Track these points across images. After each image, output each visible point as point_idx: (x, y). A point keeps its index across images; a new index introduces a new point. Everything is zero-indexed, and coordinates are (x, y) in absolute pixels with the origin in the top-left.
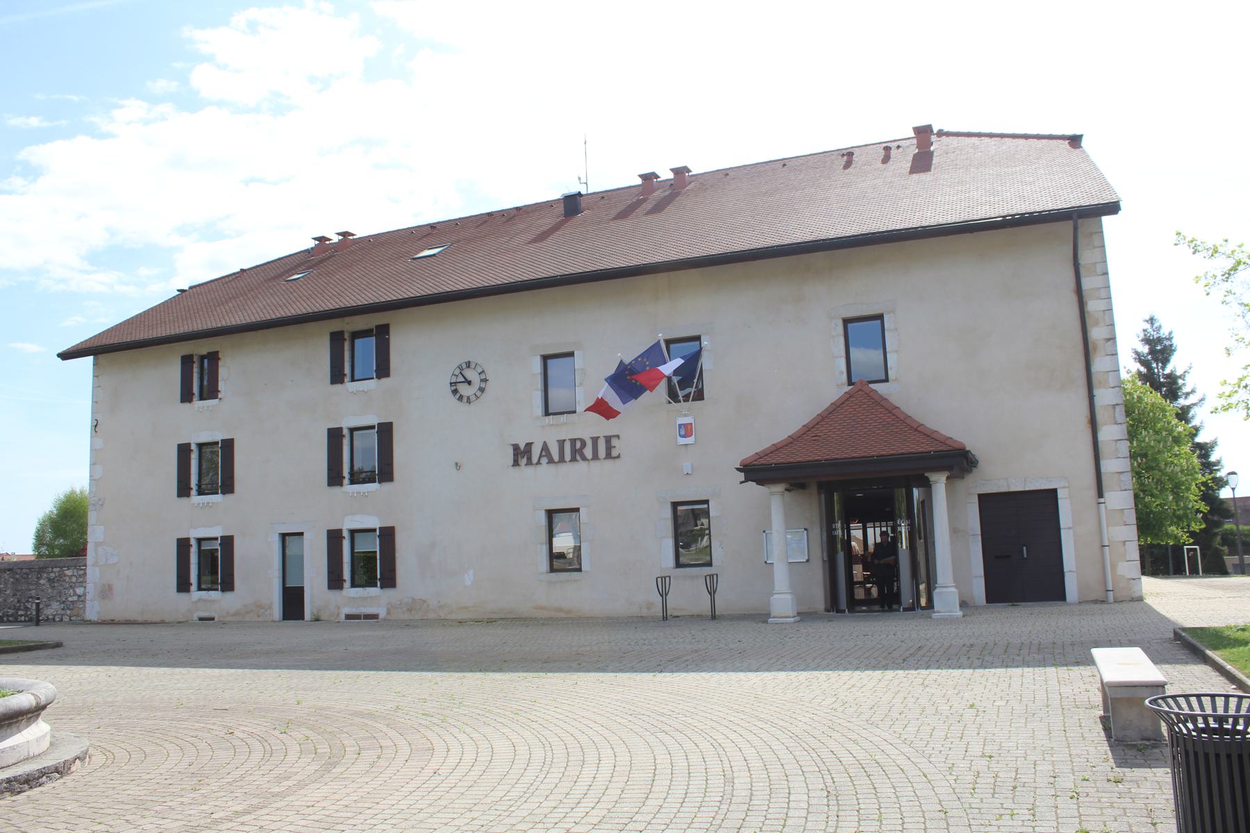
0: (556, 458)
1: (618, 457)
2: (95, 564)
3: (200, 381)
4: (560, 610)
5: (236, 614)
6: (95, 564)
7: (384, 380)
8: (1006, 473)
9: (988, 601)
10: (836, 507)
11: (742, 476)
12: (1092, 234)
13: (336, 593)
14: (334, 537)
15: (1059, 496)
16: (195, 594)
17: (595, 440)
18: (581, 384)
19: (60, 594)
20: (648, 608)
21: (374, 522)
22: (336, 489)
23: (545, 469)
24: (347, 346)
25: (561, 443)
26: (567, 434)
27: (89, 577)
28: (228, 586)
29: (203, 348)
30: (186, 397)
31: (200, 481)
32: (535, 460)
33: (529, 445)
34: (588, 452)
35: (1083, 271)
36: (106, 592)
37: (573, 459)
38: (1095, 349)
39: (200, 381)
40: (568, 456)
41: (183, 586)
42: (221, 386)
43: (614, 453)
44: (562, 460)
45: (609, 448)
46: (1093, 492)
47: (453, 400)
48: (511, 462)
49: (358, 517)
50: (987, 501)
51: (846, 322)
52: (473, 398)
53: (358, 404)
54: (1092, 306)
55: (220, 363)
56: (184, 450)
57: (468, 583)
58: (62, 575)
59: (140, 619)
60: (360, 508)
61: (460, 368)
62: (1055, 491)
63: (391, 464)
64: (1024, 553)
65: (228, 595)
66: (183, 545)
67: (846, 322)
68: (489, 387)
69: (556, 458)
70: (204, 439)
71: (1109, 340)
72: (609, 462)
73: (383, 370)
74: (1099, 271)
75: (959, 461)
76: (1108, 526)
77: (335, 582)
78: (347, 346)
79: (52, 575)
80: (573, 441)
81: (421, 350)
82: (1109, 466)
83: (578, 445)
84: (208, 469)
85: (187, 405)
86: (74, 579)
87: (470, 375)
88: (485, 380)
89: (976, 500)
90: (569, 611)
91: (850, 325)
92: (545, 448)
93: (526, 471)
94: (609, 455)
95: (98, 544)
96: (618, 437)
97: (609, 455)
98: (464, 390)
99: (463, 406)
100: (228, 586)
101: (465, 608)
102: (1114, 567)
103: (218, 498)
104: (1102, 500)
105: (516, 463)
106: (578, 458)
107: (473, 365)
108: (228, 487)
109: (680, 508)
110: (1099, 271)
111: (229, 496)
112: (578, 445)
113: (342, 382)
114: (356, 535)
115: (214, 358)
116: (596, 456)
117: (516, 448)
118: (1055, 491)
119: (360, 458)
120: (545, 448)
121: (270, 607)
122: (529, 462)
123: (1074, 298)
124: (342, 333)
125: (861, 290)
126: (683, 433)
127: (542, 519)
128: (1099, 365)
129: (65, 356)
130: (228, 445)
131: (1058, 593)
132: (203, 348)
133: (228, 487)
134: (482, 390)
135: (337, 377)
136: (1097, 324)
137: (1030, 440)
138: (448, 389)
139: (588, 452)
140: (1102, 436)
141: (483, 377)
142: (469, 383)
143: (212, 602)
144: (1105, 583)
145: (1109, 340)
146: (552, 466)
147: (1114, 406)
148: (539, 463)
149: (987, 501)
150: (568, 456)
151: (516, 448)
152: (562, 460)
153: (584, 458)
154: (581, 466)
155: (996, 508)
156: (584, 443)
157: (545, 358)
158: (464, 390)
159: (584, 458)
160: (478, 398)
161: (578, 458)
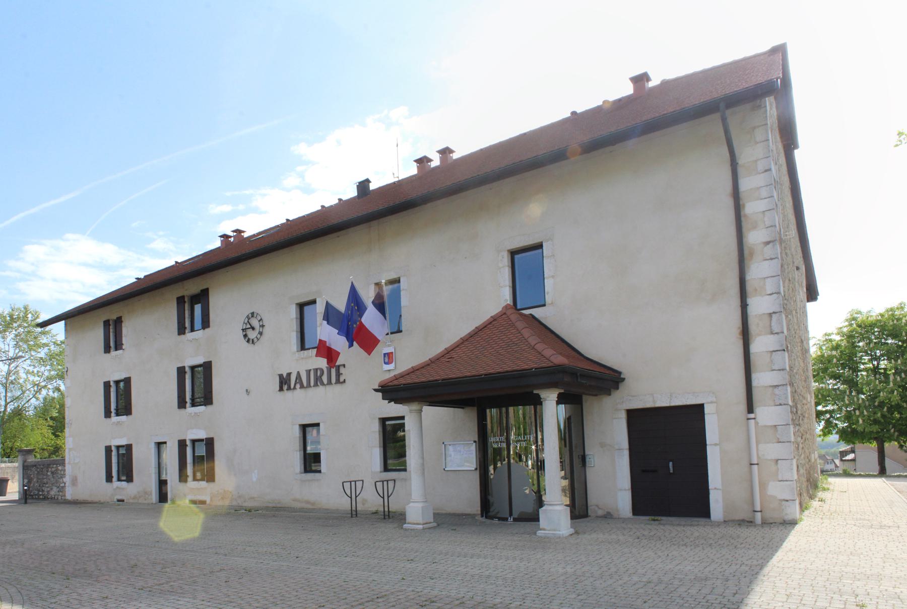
0: (305, 384)
1: (344, 381)
3: (113, 341)
4: (308, 502)
5: (134, 498)
6: (69, 463)
7: (207, 330)
8: (655, 386)
9: (638, 509)
12: (754, 128)
14: (182, 444)
15: (706, 410)
19: (57, 482)
20: (363, 504)
21: (202, 435)
22: (183, 411)
23: (299, 392)
24: (187, 306)
25: (308, 372)
27: (67, 472)
28: (130, 479)
29: (192, 288)
30: (107, 349)
32: (292, 386)
33: (289, 374)
34: (325, 379)
35: (741, 171)
36: (74, 481)
37: (316, 385)
38: (751, 254)
39: (113, 341)
41: (109, 478)
42: (124, 341)
43: (342, 380)
46: (743, 407)
48: (278, 388)
49: (194, 431)
50: (634, 416)
51: (513, 253)
52: (255, 340)
53: (192, 350)
55: (123, 325)
56: (107, 385)
57: (254, 479)
58: (57, 470)
59: (89, 499)
60: (194, 424)
61: (248, 317)
62: (701, 406)
63: (211, 392)
65: (131, 484)
66: (108, 450)
67: (513, 253)
68: (266, 330)
70: (117, 378)
72: (338, 387)
73: (206, 324)
75: (607, 380)
76: (758, 443)
77: (183, 477)
78: (187, 306)
81: (228, 303)
84: (120, 399)
85: (107, 355)
87: (255, 322)
88: (263, 326)
89: (623, 416)
90: (313, 504)
91: (516, 257)
92: (298, 373)
93: (288, 394)
95: (70, 450)
96: (344, 366)
97: (338, 381)
98: (252, 335)
99: (250, 346)
100: (130, 479)
101: (253, 498)
102: (763, 486)
104: (752, 416)
105: (281, 389)
109: (387, 423)
113: (184, 333)
115: (119, 321)
116: (330, 383)
117: (281, 376)
118: (701, 406)
119: (197, 385)
120: (298, 373)
121: (151, 494)
122: (289, 388)
123: (730, 202)
124: (183, 297)
125: (532, 215)
126: (387, 360)
127: (297, 432)
132: (192, 288)
133: (207, 400)
134: (261, 333)
135: (181, 330)
136: (755, 227)
138: (241, 334)
139: (325, 379)
140: (755, 348)
142: (253, 328)
143: (123, 489)
144: (752, 503)
147: (770, 315)
148: (295, 388)
149: (634, 416)
150: (312, 383)
151: (281, 376)
153: (323, 384)
154: (321, 389)
155: (639, 420)
158: (252, 335)
160: (258, 339)
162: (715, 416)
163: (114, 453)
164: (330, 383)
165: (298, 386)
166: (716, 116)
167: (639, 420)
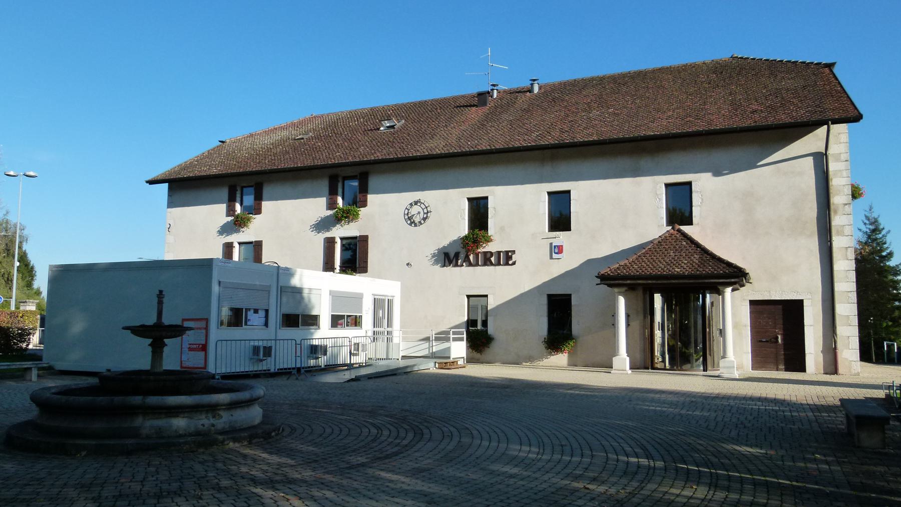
11: (598, 281)
17: (499, 253)
75: (736, 276)
83: (489, 255)
97: (507, 264)
112: (489, 255)
155: (760, 308)
164: (499, 264)
167: (760, 308)
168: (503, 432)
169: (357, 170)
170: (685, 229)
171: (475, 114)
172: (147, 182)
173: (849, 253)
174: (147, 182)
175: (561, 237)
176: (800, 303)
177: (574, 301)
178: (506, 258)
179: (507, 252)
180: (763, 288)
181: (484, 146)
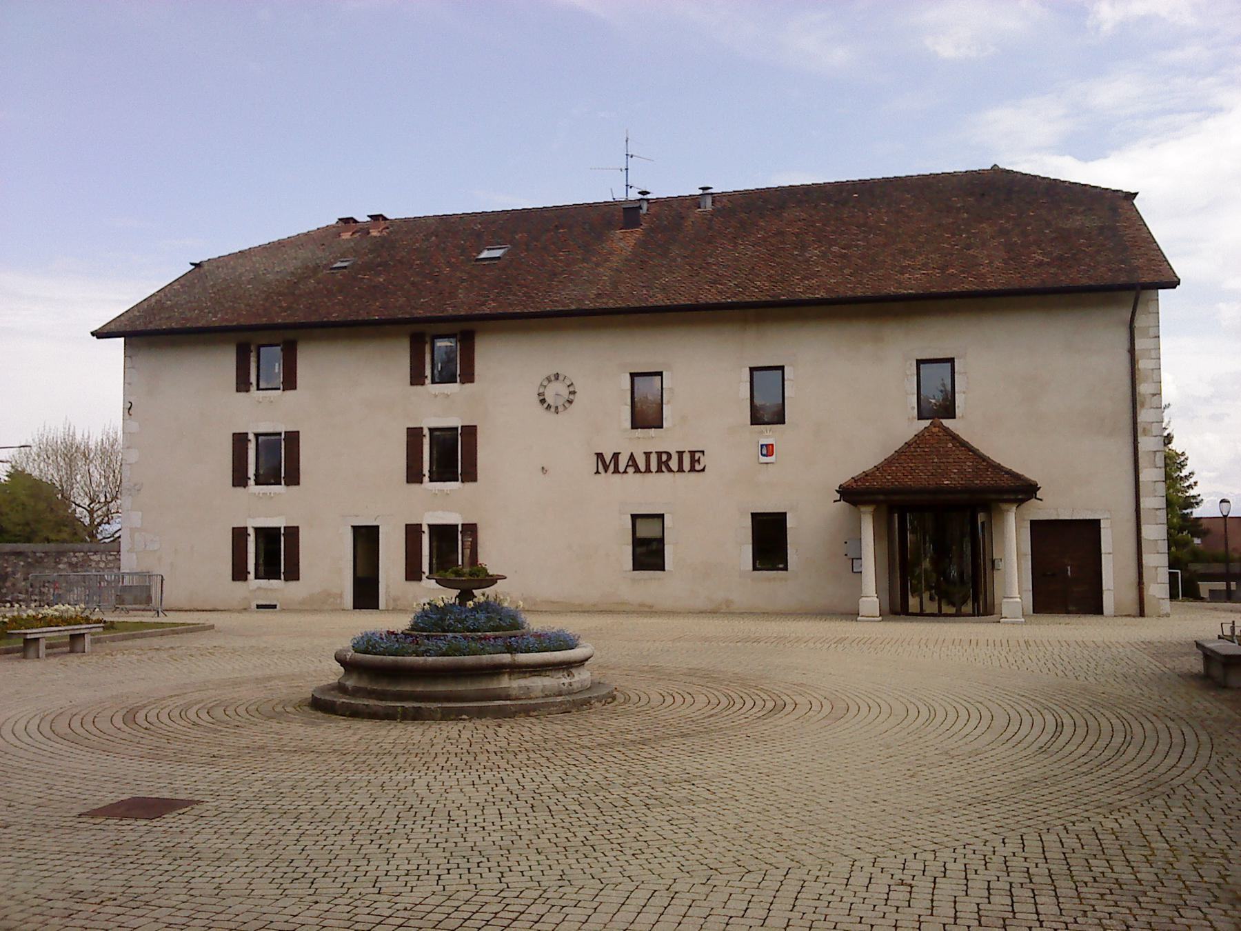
0: (643, 468)
1: (703, 470)
2: (130, 551)
6: (130, 551)
7: (468, 385)
10: (419, 689)
11: (838, 496)
13: (414, 584)
14: (413, 532)
16: (253, 582)
17: (680, 454)
18: (668, 402)
22: (415, 487)
26: (654, 447)
28: (293, 574)
31: (257, 470)
32: (621, 469)
33: (616, 456)
34: (674, 464)
37: (659, 470)
40: (654, 467)
41: (239, 573)
43: (698, 467)
44: (648, 470)
45: (694, 461)
47: (540, 409)
49: (440, 513)
54: (1142, 364)
60: (441, 504)
62: (1098, 521)
64: (1069, 571)
65: (292, 584)
69: (643, 468)
71: (1154, 395)
72: (693, 475)
74: (1152, 333)
75: (1025, 490)
77: (413, 573)
79: (74, 560)
80: (659, 454)
82: (1147, 503)
83: (664, 457)
84: (275, 460)
86: (102, 565)
92: (632, 457)
94: (692, 469)
97: (692, 469)
99: (550, 416)
103: (281, 489)
106: (664, 469)
107: (561, 378)
108: (293, 478)
110: (1152, 333)
111: (293, 488)
112: (664, 457)
114: (639, 521)
118: (1098, 521)
120: (632, 457)
121: (341, 596)
122: (616, 471)
126: (765, 452)
128: (1144, 416)
129: (99, 334)
130: (293, 438)
131: (1097, 609)
133: (293, 478)
137: (1077, 479)
139: (674, 464)
141: (571, 389)
145: (1154, 395)
146: (638, 475)
149: (1039, 528)
150: (654, 467)
152: (648, 470)
153: (670, 470)
154: (666, 476)
155: (1042, 531)
156: (669, 456)
157: (633, 376)
159: (670, 470)
161: (664, 469)
162: (1109, 531)
163: (251, 540)
164: (681, 470)
165: (631, 470)
166: (1133, 293)
167: (1042, 531)
168: (919, 700)
169: (457, 327)
170: (946, 423)
171: (624, 242)
172: (93, 334)
173: (1157, 459)
174: (93, 334)
175: (769, 435)
176: (1094, 525)
177: (790, 523)
178: (693, 462)
179: (692, 453)
180: (1051, 507)
181: (659, 299)
